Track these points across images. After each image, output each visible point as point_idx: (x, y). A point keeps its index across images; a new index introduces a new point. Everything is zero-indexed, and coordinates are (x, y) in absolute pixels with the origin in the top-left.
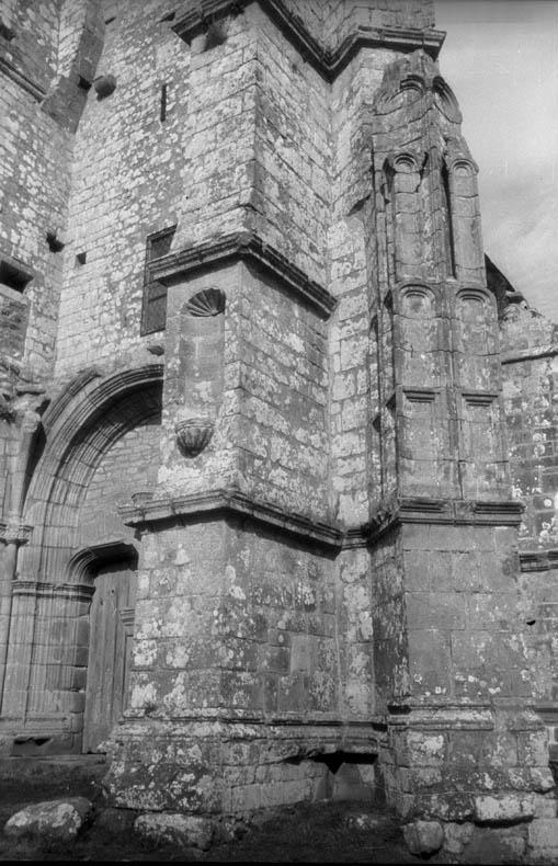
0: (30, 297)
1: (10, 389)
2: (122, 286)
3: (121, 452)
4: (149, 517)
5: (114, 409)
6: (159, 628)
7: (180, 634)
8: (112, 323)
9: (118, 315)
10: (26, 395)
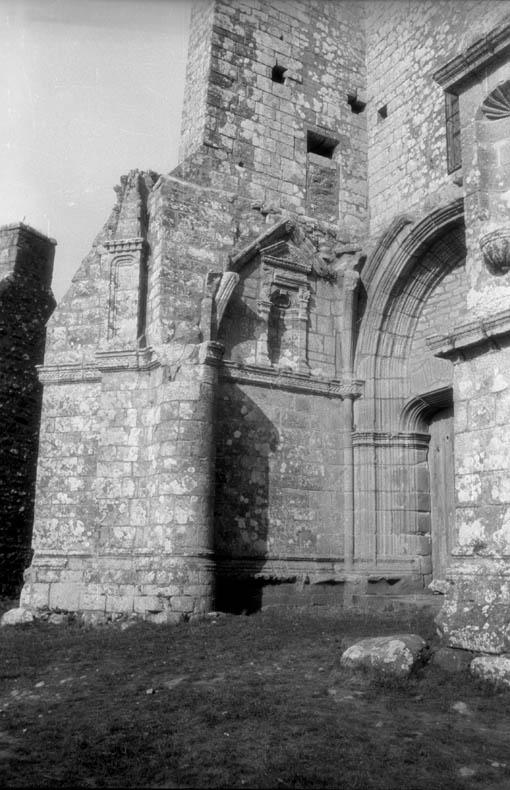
0: (339, 162)
1: (329, 252)
2: (424, 129)
3: (441, 298)
4: (458, 344)
5: (429, 254)
6: (481, 461)
7: (505, 466)
8: (419, 169)
9: (424, 159)
10: (345, 255)
